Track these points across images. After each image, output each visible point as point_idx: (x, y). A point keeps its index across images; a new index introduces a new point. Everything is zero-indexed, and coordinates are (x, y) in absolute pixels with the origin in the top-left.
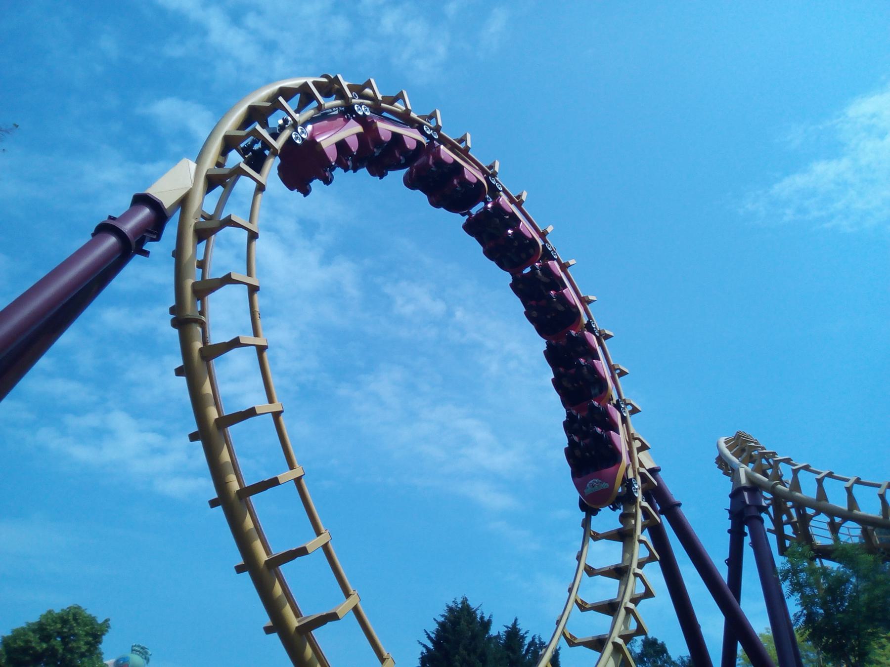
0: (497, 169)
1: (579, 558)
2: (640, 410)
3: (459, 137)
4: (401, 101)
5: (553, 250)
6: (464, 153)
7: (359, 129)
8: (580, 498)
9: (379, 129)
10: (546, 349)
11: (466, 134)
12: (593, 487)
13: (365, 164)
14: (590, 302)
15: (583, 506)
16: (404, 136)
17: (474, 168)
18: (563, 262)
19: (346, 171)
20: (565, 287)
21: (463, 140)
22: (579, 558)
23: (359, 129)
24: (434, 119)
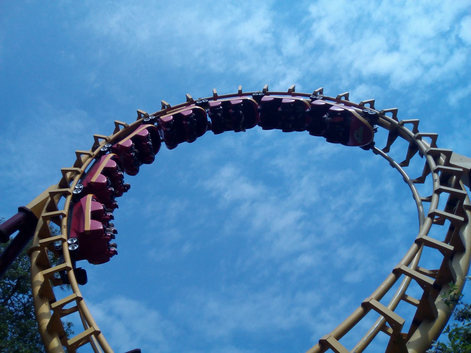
0: (167, 104)
1: (393, 165)
2: (374, 100)
3: (137, 116)
4: (99, 140)
5: (258, 93)
6: (129, 130)
7: (90, 197)
8: (360, 147)
9: (96, 182)
10: (326, 139)
11: (162, 102)
12: (359, 136)
13: (103, 230)
14: (293, 90)
15: (366, 148)
16: (181, 113)
17: (184, 108)
18: (335, 98)
19: (114, 238)
20: (281, 99)
21: (164, 106)
22: (393, 165)
23: (90, 197)
24: (120, 126)
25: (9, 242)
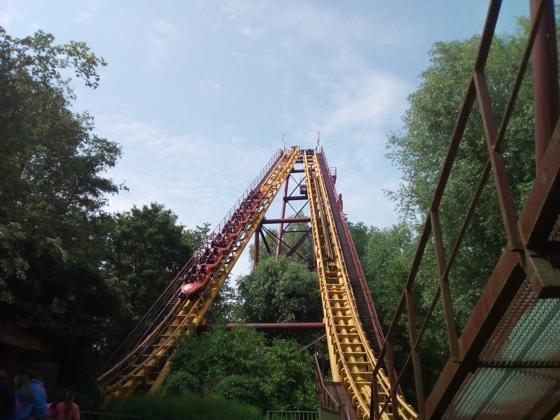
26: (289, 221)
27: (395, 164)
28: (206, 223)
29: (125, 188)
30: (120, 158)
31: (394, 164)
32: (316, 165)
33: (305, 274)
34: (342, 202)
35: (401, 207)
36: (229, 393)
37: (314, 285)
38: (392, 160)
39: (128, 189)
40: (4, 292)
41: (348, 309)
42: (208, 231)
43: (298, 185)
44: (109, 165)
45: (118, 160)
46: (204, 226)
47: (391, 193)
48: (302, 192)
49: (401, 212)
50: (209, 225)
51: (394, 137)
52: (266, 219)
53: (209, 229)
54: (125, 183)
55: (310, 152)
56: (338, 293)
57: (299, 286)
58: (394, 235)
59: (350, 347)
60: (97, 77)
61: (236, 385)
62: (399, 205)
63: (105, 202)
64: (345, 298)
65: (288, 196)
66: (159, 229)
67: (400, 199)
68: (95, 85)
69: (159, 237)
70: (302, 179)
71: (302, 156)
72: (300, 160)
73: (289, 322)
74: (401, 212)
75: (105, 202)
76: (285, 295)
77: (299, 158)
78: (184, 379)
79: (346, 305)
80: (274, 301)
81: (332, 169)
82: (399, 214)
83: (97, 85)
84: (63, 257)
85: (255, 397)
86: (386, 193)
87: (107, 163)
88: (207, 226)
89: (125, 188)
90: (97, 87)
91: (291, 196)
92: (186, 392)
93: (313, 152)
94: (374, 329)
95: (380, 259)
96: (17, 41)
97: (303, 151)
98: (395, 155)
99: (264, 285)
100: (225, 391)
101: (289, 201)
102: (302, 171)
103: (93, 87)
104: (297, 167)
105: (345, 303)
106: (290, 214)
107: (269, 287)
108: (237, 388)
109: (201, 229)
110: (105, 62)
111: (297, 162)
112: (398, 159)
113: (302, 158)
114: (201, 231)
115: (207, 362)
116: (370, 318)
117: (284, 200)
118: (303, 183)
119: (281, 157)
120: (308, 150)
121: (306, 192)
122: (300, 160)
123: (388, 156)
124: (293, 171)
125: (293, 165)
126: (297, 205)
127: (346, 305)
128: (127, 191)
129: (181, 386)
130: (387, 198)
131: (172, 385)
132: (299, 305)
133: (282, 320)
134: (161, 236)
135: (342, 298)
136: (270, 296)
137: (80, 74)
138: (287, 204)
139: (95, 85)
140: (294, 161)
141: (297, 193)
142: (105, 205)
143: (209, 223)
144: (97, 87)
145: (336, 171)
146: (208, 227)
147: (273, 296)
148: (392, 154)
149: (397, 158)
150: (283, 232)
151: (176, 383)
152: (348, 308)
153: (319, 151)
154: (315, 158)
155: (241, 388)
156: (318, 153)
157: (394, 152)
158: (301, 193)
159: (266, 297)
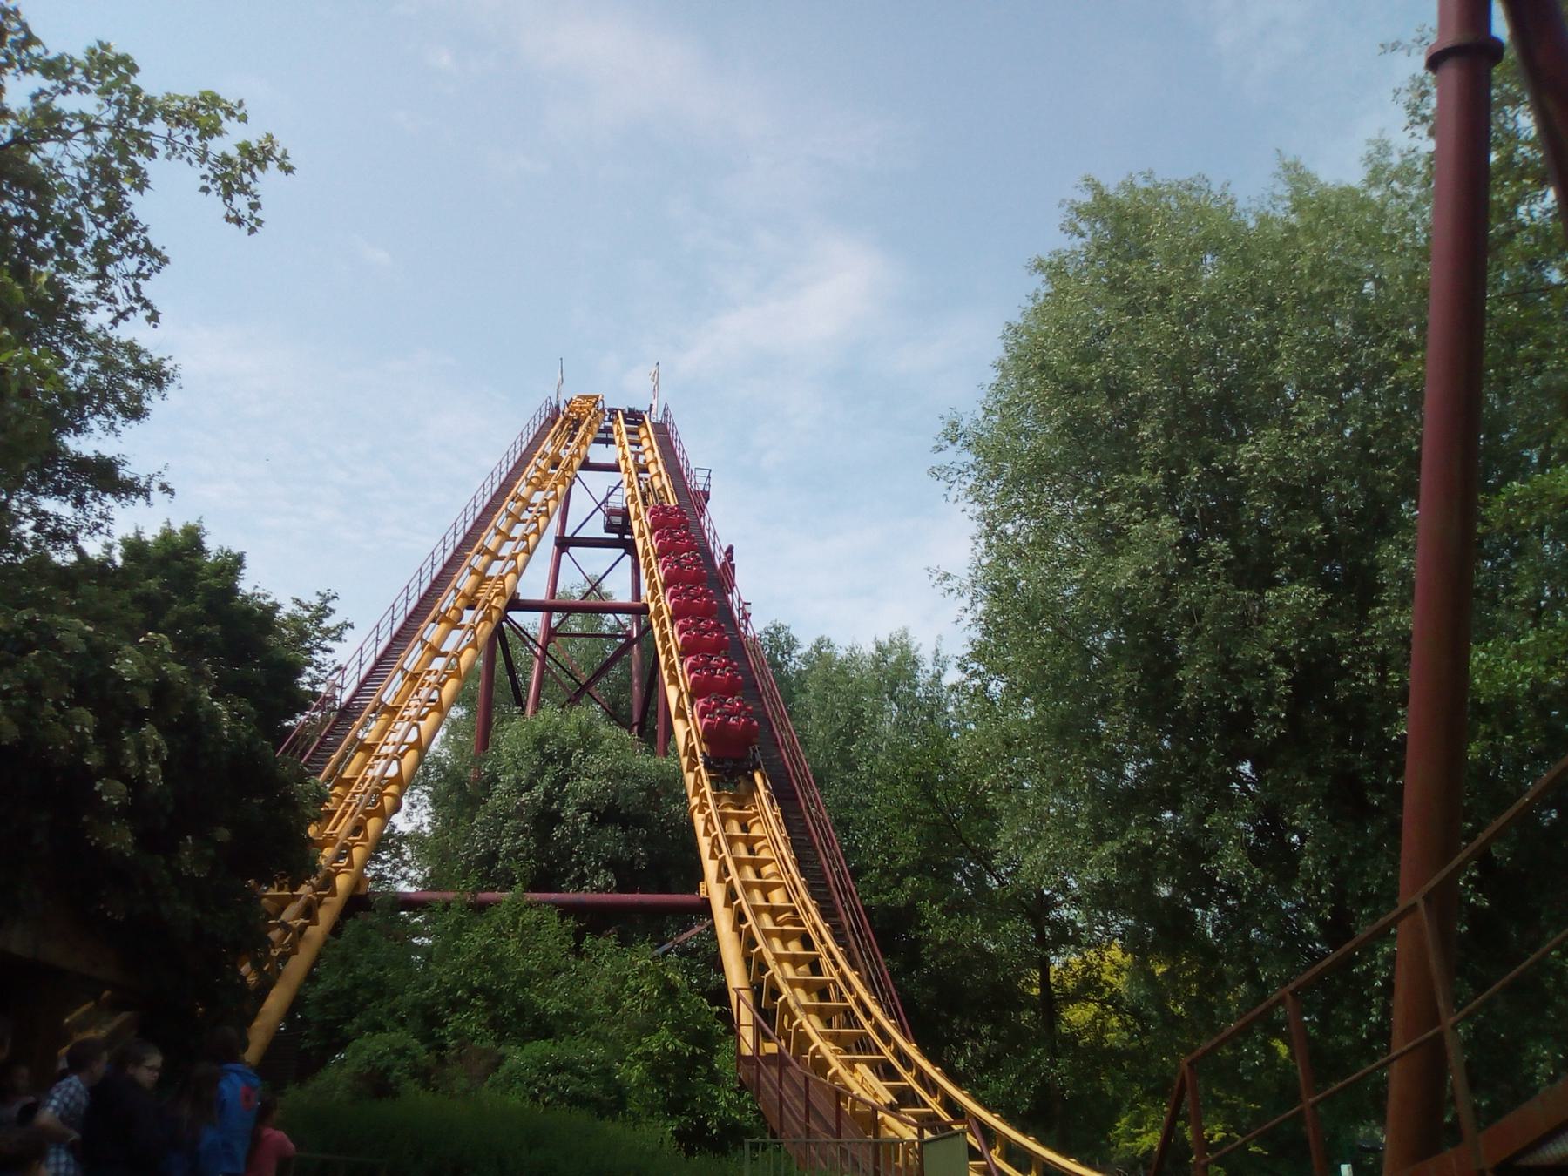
25: (1511, 55)
26: (569, 609)
27: (955, 498)
28: (323, 591)
29: (164, 488)
30: (160, 398)
31: (952, 496)
32: (651, 455)
33: (645, 762)
34: (733, 566)
35: (972, 617)
36: (541, 1090)
37: (672, 787)
38: (948, 485)
39: (171, 492)
40: (113, 823)
41: (769, 861)
42: (327, 616)
43: (599, 506)
44: (126, 416)
45: (154, 402)
46: (316, 601)
47: (947, 576)
48: (609, 528)
49: (973, 628)
50: (334, 597)
51: (955, 425)
52: (520, 598)
53: (331, 610)
54: (163, 472)
55: (635, 418)
56: (739, 818)
57: (628, 792)
58: (877, 668)
59: (789, 962)
60: (252, 200)
61: (557, 1069)
62: (966, 610)
63: (101, 525)
64: (756, 831)
65: (568, 534)
66: (210, 607)
67: (968, 595)
68: (253, 223)
69: (209, 629)
70: (611, 489)
71: (610, 424)
72: (603, 436)
73: (598, 890)
74: (973, 628)
75: (101, 525)
76: (591, 819)
77: (600, 431)
78: (401, 1053)
79: (760, 850)
80: (557, 833)
81: (698, 472)
82: (967, 633)
83: (260, 222)
84: (225, 723)
85: (606, 1098)
86: (936, 577)
87: (121, 408)
88: (327, 601)
89: (164, 488)
90: (258, 228)
91: (576, 535)
92: (411, 1086)
93: (643, 418)
94: (840, 914)
95: (839, 733)
96: (30, 63)
97: (613, 411)
98: (955, 472)
99: (529, 788)
100: (529, 1084)
101: (571, 550)
102: (615, 468)
103: (246, 228)
104: (599, 454)
105: (758, 846)
106: (572, 584)
107: (547, 793)
108: (565, 1076)
109: (307, 608)
110: (288, 162)
111: (597, 441)
112: (962, 486)
113: (609, 430)
114: (307, 614)
115: (439, 1004)
116: (827, 885)
117: (556, 544)
118: (617, 502)
119: (554, 422)
120: (627, 411)
121: (625, 528)
122: (603, 436)
123: (937, 473)
124: (587, 466)
125: (587, 447)
126: (596, 561)
127: (760, 850)
128: (168, 495)
129: (395, 1073)
130: (940, 589)
131: (368, 1069)
132: (628, 845)
133: (580, 880)
134: (215, 630)
135: (749, 832)
136: (546, 819)
137: (212, 187)
138: (565, 555)
139: (253, 223)
140: (590, 438)
141: (596, 529)
142: (101, 533)
143: (332, 593)
144: (258, 228)
145: (709, 477)
146: (330, 605)
147: (555, 819)
148: (946, 468)
149: (960, 481)
150: (551, 633)
151: (379, 1064)
152: (771, 857)
153: (657, 417)
154: (648, 438)
155: (571, 1074)
156: (654, 421)
157: (953, 465)
158: (607, 531)
159: (536, 821)
